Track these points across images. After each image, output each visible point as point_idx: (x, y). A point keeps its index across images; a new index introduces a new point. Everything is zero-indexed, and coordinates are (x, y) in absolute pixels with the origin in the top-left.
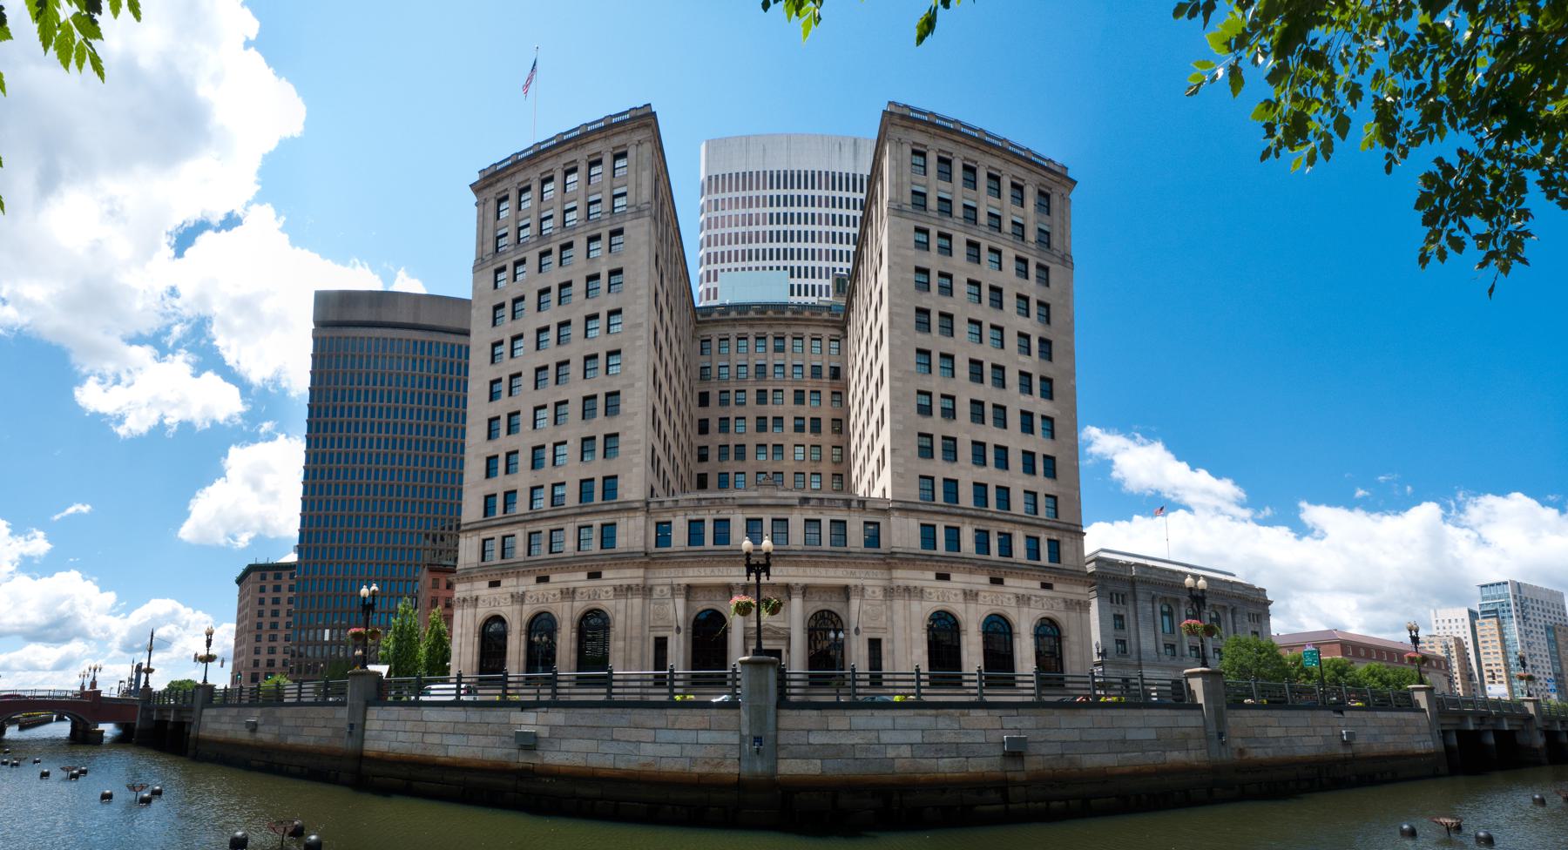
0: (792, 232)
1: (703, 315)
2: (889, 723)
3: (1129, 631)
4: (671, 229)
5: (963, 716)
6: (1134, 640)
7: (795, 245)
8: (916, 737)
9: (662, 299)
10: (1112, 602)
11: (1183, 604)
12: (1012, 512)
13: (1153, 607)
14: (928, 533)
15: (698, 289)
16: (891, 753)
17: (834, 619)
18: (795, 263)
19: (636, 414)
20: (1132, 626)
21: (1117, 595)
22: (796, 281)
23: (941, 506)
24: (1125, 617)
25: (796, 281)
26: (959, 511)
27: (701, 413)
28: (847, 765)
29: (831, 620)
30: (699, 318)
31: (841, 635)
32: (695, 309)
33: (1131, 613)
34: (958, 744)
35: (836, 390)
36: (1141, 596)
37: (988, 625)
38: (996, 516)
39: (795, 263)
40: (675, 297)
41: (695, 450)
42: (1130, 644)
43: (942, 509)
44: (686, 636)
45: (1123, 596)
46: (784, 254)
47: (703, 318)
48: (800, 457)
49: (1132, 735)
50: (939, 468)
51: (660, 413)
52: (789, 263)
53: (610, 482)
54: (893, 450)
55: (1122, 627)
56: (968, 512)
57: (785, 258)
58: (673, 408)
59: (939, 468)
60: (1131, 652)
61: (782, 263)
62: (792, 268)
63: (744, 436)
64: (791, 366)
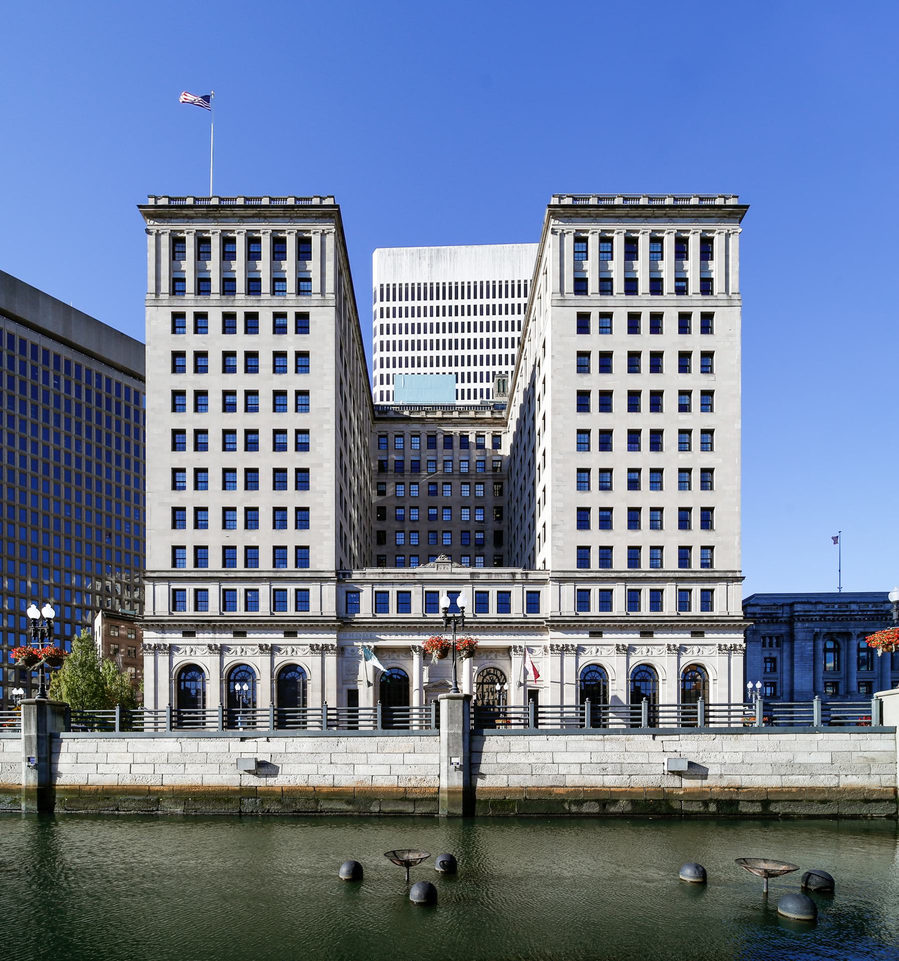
0: (456, 357)
1: (380, 412)
2: (562, 747)
3: (782, 673)
4: (353, 327)
5: (628, 740)
6: (786, 681)
7: (459, 353)
8: (585, 758)
9: (346, 389)
10: (764, 645)
11: (855, 637)
12: (665, 568)
13: (814, 646)
14: (583, 600)
15: (376, 390)
16: (563, 770)
17: (499, 673)
18: (459, 369)
19: (325, 492)
20: (786, 667)
21: (771, 638)
22: (460, 386)
23: (597, 572)
24: (778, 660)
25: (460, 386)
26: (613, 575)
27: (378, 526)
28: (525, 779)
29: (496, 675)
30: (376, 413)
31: (506, 687)
32: (372, 405)
33: (785, 654)
34: (622, 763)
35: (497, 481)
36: (800, 635)
37: (636, 674)
38: (649, 575)
39: (459, 369)
40: (356, 391)
41: (375, 535)
42: (782, 686)
43: (598, 575)
44: (375, 690)
45: (777, 638)
46: (454, 361)
47: (381, 414)
48: (480, 494)
49: (801, 759)
50: (595, 538)
51: (346, 529)
52: (454, 369)
53: (303, 554)
54: (554, 526)
55: (774, 669)
56: (622, 575)
57: (450, 365)
58: (356, 492)
59: (595, 538)
60: (782, 694)
61: (447, 369)
62: (457, 374)
63: (417, 523)
64: (458, 461)
